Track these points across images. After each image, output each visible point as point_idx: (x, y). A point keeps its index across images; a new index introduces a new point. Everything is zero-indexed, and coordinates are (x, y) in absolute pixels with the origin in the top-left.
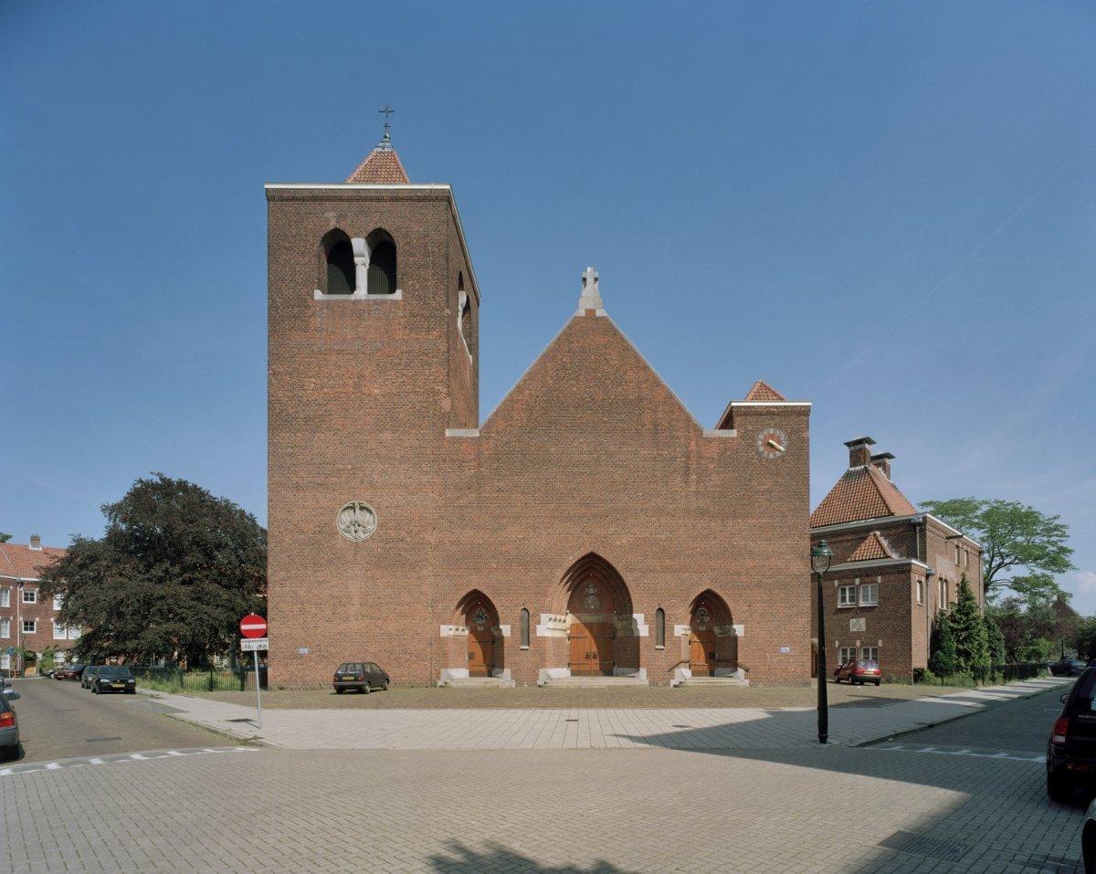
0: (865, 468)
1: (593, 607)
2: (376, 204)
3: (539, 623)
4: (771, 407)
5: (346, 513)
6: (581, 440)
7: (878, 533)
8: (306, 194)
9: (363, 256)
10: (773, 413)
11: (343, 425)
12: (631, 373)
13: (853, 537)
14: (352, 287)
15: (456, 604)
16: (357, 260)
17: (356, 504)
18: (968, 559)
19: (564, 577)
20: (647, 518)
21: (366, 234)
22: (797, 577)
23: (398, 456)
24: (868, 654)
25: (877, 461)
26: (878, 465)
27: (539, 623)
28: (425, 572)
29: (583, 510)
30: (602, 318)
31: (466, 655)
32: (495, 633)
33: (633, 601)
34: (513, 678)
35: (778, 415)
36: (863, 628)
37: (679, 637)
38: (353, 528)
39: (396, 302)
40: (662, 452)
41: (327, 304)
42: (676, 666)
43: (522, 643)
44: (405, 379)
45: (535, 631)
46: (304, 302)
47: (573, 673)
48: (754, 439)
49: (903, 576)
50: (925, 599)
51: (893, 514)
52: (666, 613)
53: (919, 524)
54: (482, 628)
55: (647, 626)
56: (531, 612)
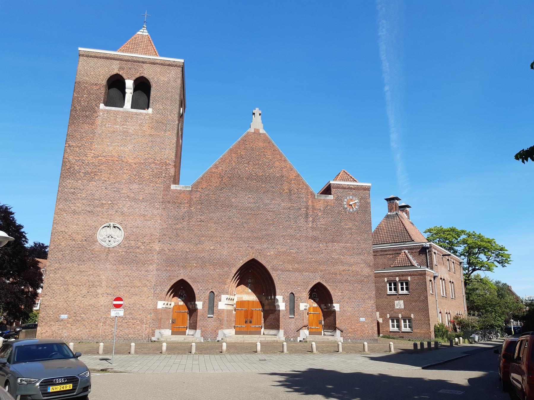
0: (396, 213)
3: (220, 301)
4: (351, 185)
7: (407, 251)
8: (102, 55)
9: (131, 89)
10: (352, 188)
11: (108, 178)
12: (277, 163)
13: (393, 252)
15: (169, 288)
16: (127, 90)
18: (454, 267)
19: (309, 292)
20: (285, 241)
22: (367, 277)
23: (141, 198)
24: (406, 322)
25: (402, 209)
26: (403, 211)
27: (220, 301)
28: (151, 267)
29: (249, 234)
30: (263, 134)
31: (171, 320)
33: (276, 288)
34: (202, 336)
35: (354, 189)
37: (303, 311)
38: (107, 239)
42: (300, 329)
43: (209, 314)
45: (217, 305)
46: (94, 110)
47: (237, 333)
48: (342, 201)
49: (422, 277)
50: (434, 290)
51: (413, 241)
52: (295, 296)
53: (428, 248)
55: (284, 304)
56: (216, 294)
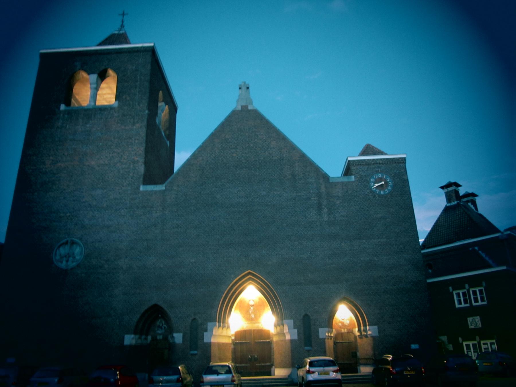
6: (240, 188)
32: (171, 341)
40: (300, 194)
44: (115, 154)
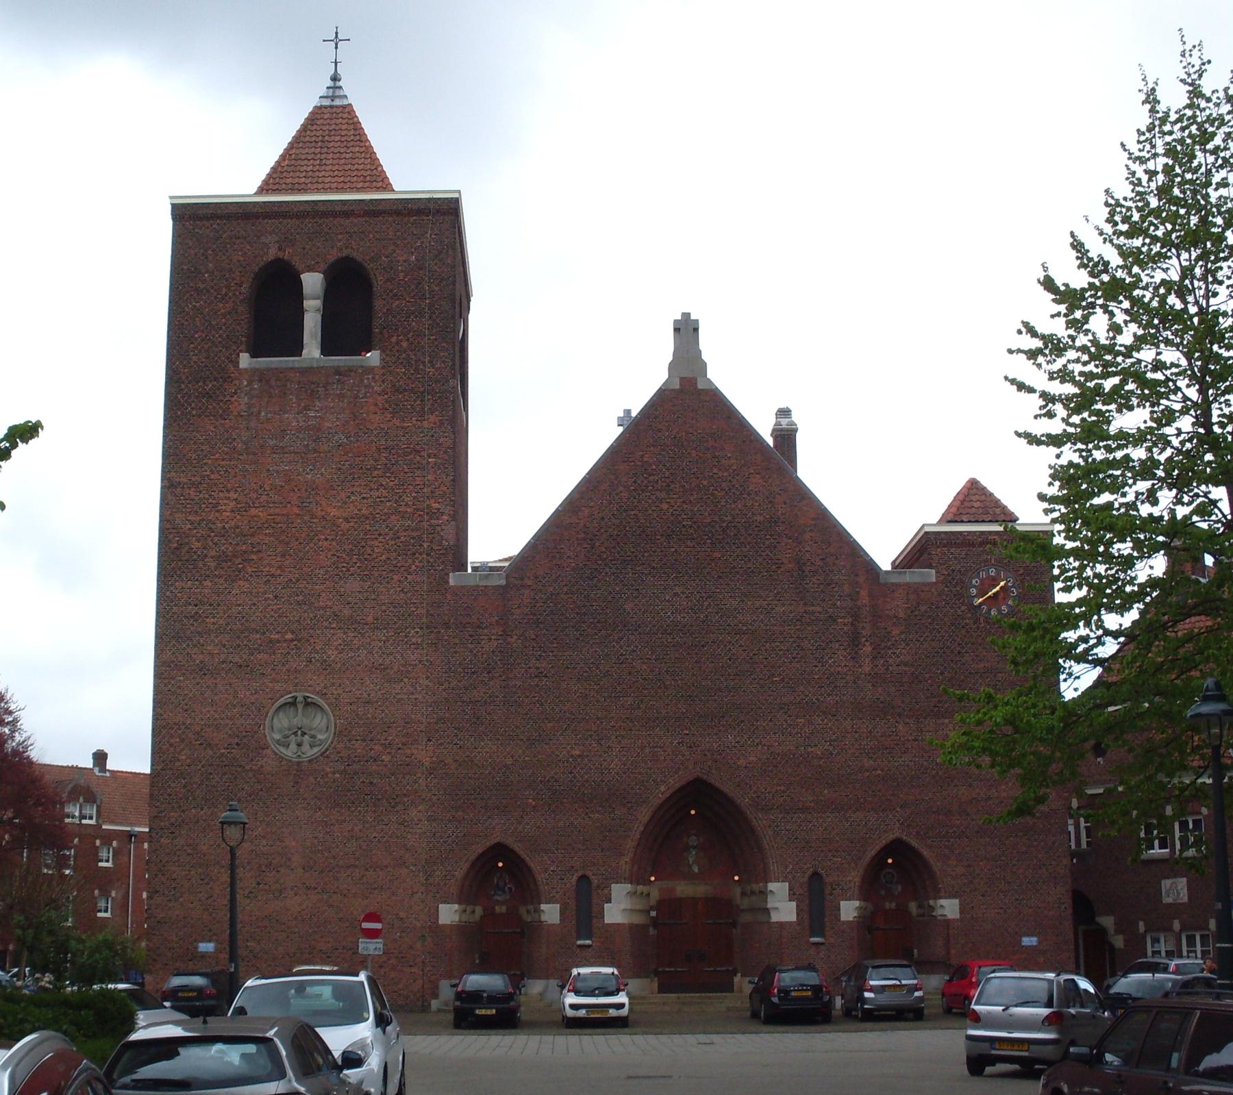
1: (696, 870)
2: (342, 221)
3: (609, 901)
4: (990, 533)
5: (281, 715)
6: (677, 590)
11: (280, 567)
14: (296, 348)
16: (307, 304)
17: (300, 699)
21: (324, 266)
23: (370, 619)
27: (609, 901)
28: (413, 813)
36: (1184, 897)
39: (369, 370)
41: (261, 375)
54: (504, 909)
